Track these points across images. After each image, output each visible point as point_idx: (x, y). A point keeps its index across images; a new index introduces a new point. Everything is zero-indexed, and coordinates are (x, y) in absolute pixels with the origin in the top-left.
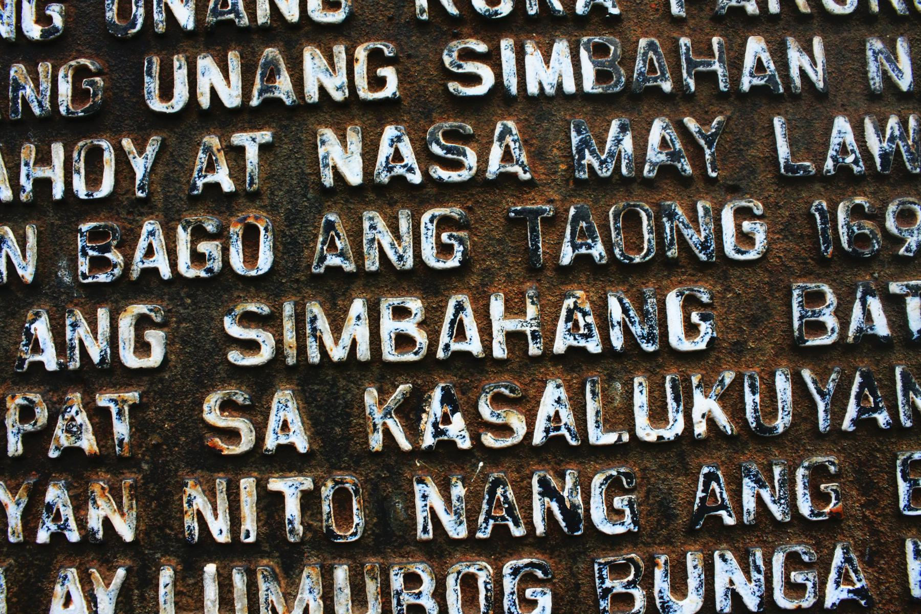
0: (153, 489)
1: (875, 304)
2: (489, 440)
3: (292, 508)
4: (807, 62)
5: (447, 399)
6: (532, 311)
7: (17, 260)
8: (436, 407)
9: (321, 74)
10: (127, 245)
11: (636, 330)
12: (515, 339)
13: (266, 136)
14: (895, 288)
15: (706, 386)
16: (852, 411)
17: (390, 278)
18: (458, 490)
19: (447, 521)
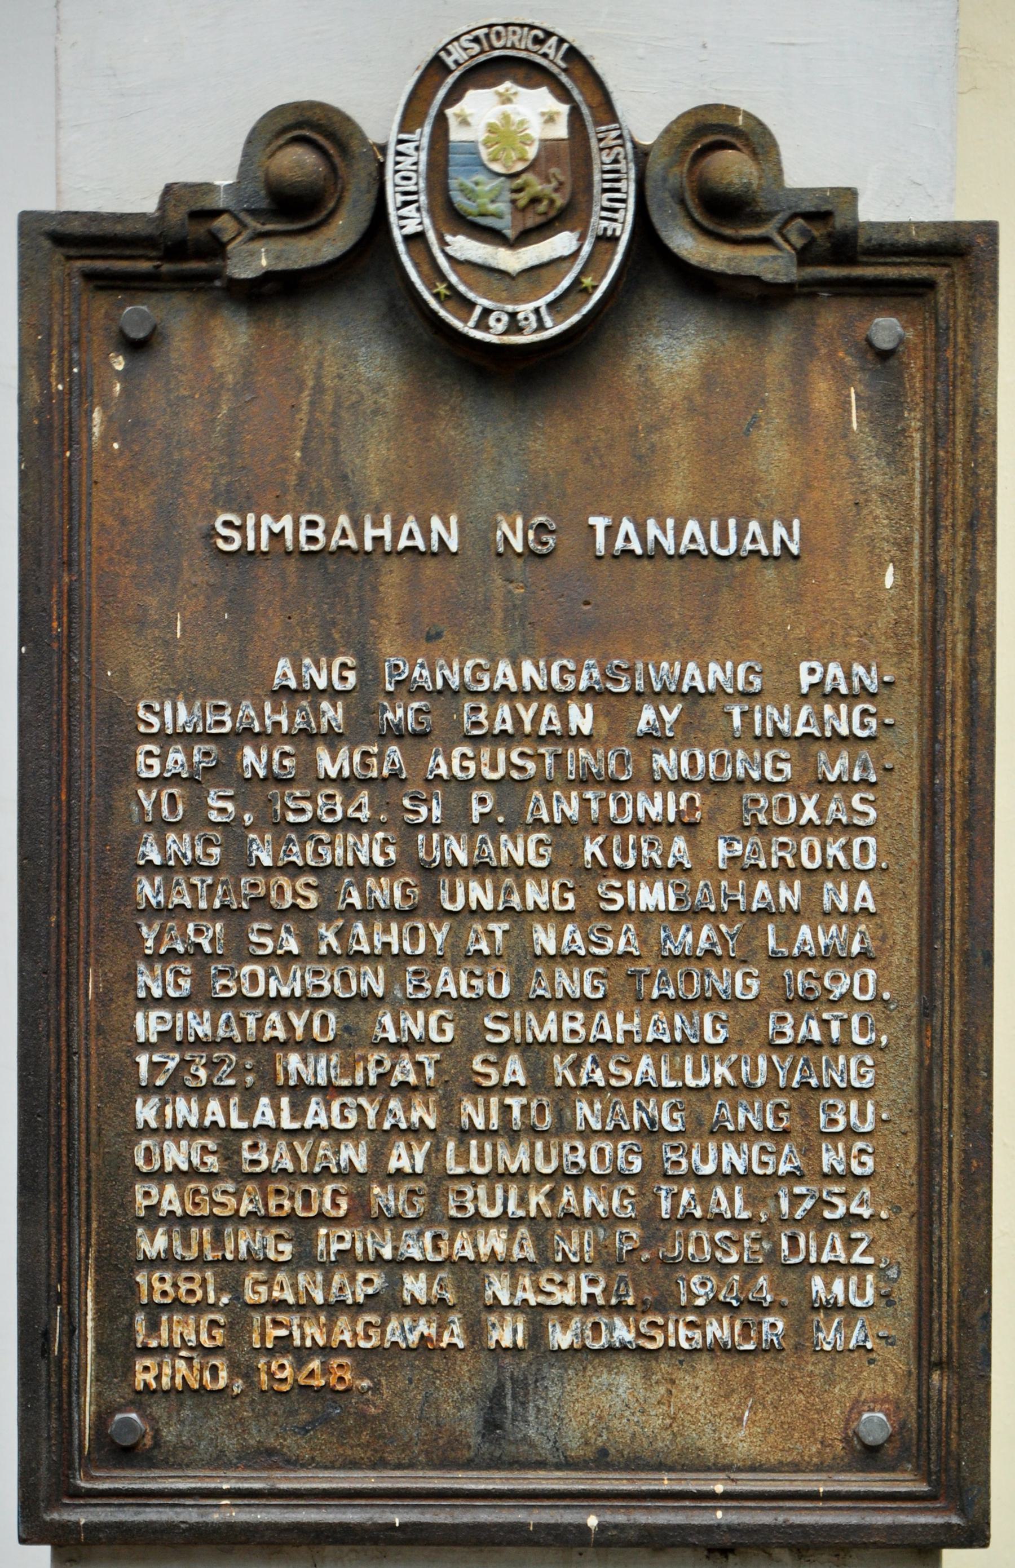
0: (444, 1103)
1: (814, 1024)
2: (614, 1082)
3: (516, 1112)
4: (790, 895)
5: (594, 1061)
6: (637, 1020)
7: (373, 985)
8: (588, 1065)
9: (535, 895)
10: (434, 978)
11: (688, 1032)
12: (628, 1033)
13: (506, 926)
14: (825, 1016)
15: (722, 1061)
16: (797, 1077)
17: (570, 1001)
18: (598, 1106)
19: (592, 1121)
